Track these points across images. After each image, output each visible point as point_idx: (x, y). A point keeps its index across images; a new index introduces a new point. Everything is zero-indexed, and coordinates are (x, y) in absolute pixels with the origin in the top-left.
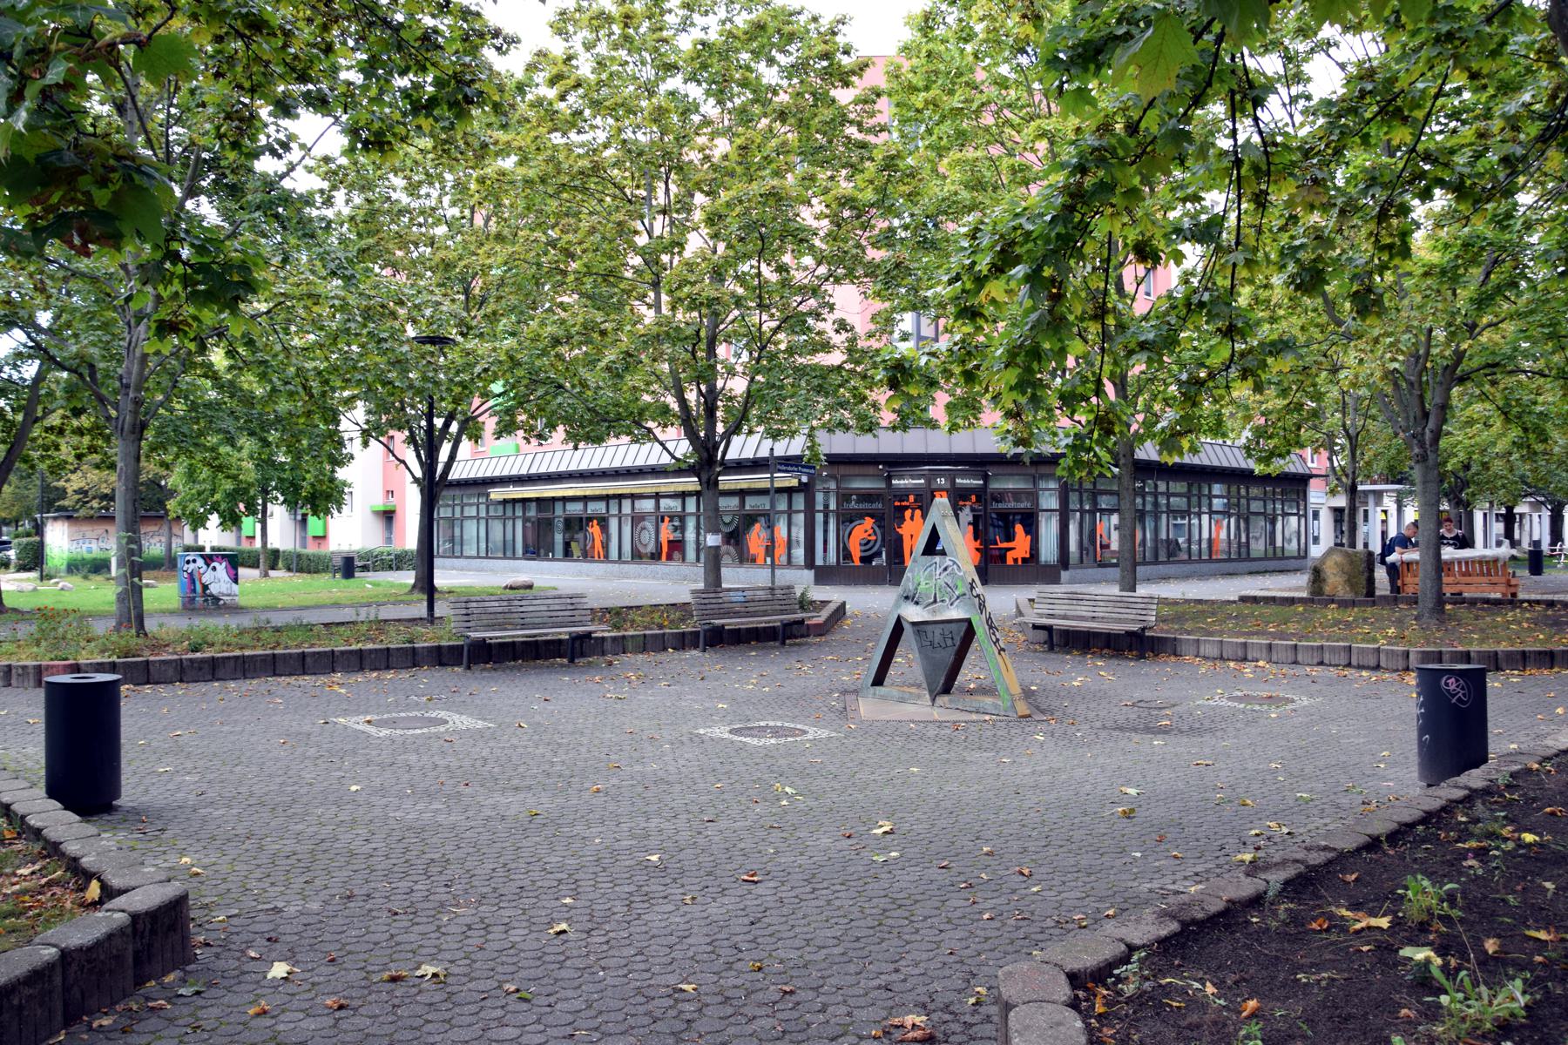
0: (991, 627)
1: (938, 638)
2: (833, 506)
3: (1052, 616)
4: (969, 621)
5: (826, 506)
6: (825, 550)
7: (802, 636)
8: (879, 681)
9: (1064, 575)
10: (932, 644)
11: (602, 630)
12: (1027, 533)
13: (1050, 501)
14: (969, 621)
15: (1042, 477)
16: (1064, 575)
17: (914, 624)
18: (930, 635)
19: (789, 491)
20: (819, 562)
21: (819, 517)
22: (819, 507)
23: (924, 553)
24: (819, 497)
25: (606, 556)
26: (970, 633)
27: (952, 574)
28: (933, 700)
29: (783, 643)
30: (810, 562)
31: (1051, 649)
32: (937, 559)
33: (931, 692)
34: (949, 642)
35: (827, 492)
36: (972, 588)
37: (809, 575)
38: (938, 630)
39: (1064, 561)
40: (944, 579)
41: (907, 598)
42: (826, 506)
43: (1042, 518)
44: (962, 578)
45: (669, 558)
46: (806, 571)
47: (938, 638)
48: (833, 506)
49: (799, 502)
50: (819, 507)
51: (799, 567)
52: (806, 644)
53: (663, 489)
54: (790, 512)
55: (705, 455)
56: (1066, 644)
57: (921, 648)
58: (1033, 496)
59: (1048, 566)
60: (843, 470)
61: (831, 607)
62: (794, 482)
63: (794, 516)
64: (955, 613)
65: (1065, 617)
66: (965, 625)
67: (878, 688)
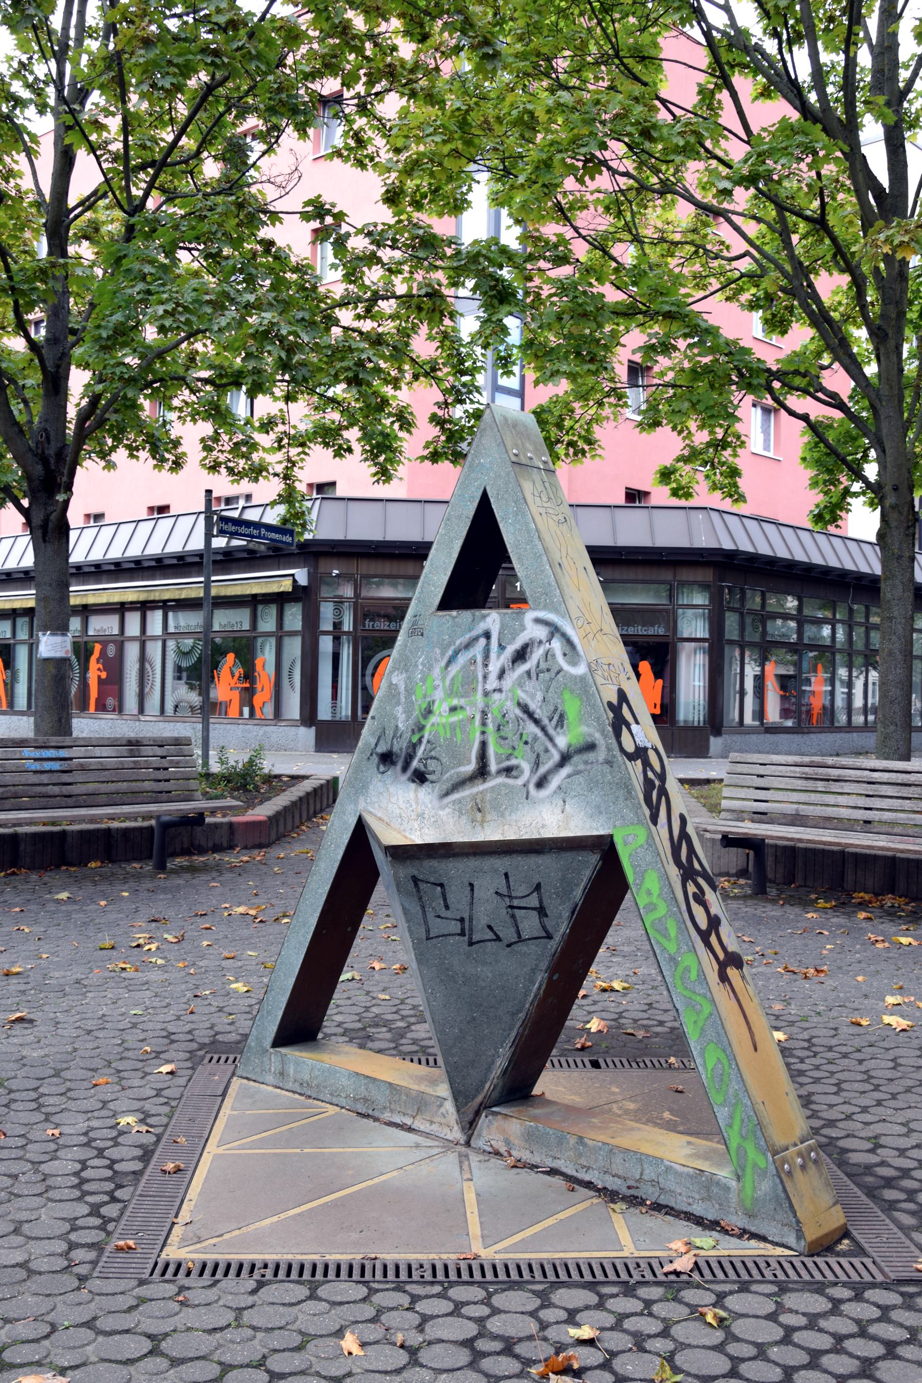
0: (688, 873)
1: (487, 909)
2: (347, 626)
3: (760, 816)
4: (605, 848)
5: (337, 625)
6: (335, 696)
7: (217, 849)
8: (301, 1025)
9: (715, 743)
10: (465, 928)
11: (223, 810)
12: (658, 675)
13: (694, 626)
14: (605, 848)
15: (683, 584)
16: (715, 743)
17: (400, 853)
18: (458, 896)
19: (280, 599)
20: (324, 713)
21: (326, 644)
22: (326, 626)
23: (446, 604)
24: (327, 611)
25: (11, 704)
26: (607, 884)
27: (547, 671)
28: (470, 1126)
29: (161, 867)
30: (309, 716)
31: (760, 891)
32: (492, 619)
33: (460, 1096)
34: (530, 924)
35: (339, 602)
36: (619, 724)
37: (308, 735)
38: (488, 878)
39: (715, 720)
40: (517, 689)
41: (387, 758)
42: (337, 625)
43: (686, 649)
44: (583, 687)
45: (101, 707)
46: (303, 730)
47: (487, 909)
48: (347, 626)
49: (294, 617)
50: (326, 626)
51: (292, 723)
52: (218, 868)
53: (91, 600)
54: (280, 635)
55: (39, 470)
56: (790, 879)
57: (425, 941)
58: (669, 616)
59: (690, 729)
60: (366, 567)
61: (307, 786)
62: (286, 586)
63: (287, 641)
64: (552, 817)
65: (797, 820)
66: (594, 859)
67: (291, 1053)
